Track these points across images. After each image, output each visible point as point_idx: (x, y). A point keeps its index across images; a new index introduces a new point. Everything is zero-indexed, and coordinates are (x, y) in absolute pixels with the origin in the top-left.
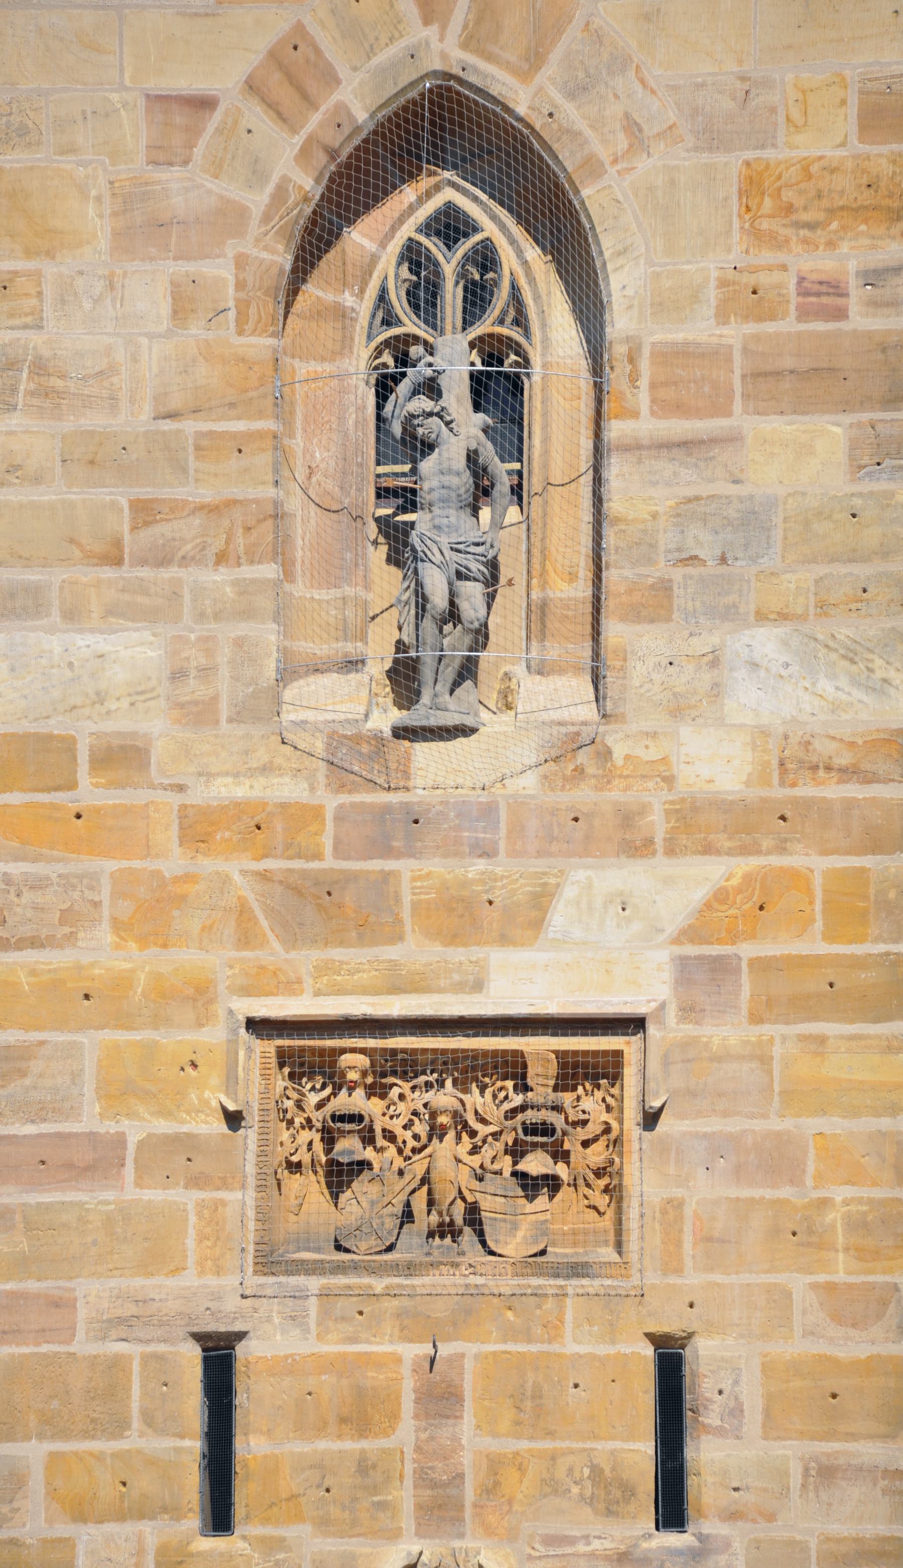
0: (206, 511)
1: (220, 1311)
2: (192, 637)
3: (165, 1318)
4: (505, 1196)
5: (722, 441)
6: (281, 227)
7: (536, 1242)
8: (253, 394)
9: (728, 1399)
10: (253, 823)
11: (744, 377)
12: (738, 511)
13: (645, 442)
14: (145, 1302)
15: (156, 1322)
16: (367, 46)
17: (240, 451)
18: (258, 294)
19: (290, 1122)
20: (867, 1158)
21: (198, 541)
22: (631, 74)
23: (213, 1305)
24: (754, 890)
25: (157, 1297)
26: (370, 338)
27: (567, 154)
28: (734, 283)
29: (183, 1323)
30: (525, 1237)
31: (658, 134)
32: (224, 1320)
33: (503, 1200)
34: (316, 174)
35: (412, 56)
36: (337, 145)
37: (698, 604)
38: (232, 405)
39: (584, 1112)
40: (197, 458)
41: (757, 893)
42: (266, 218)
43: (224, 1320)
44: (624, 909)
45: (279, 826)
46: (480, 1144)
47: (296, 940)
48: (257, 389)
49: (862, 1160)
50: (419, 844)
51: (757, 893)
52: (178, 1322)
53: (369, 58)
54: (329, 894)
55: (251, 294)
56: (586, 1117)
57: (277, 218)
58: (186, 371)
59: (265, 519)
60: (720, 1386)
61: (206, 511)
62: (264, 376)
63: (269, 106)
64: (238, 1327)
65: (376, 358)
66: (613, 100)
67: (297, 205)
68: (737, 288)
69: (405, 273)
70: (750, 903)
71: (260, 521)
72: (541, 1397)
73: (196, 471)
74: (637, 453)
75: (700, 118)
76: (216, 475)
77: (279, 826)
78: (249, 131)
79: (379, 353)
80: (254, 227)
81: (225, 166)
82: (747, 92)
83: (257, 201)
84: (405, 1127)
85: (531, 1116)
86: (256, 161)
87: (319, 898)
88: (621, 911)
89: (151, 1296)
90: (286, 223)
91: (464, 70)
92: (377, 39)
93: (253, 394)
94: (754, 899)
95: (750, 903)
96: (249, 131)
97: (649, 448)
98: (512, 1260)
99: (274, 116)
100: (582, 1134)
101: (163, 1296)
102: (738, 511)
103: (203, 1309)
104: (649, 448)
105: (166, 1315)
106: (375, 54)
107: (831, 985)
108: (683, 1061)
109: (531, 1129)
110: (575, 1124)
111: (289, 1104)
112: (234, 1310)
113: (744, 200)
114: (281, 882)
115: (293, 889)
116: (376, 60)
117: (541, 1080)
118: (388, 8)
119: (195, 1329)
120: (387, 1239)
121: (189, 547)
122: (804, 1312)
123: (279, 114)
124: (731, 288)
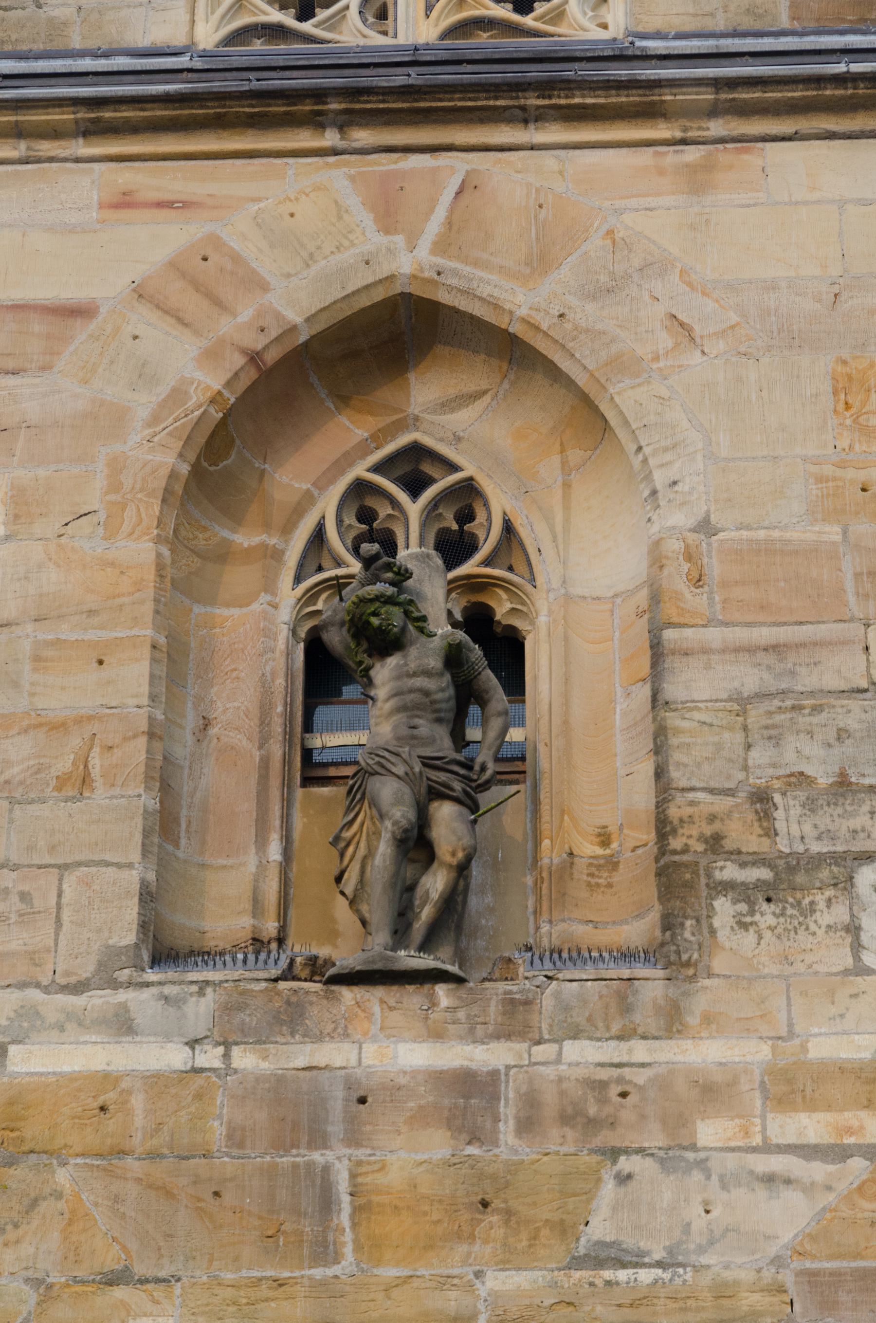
0: (45, 729)
2: (33, 366)
5: (830, 643)
6: (176, 428)
8: (126, 600)
10: (96, 1104)
11: (857, 576)
12: (860, 721)
13: (714, 646)
16: (304, 254)
17: (101, 662)
18: (139, 496)
21: (32, 763)
22: (675, 277)
26: (298, 579)
27: (587, 352)
28: (835, 479)
31: (715, 334)
34: (229, 375)
35: (367, 263)
36: (259, 347)
37: (807, 828)
38: (91, 613)
40: (35, 670)
42: (155, 419)
44: (707, 1212)
45: (138, 1102)
47: (161, 1256)
48: (131, 594)
50: (368, 1128)
53: (308, 266)
55: (129, 496)
57: (171, 420)
58: (26, 578)
59: (135, 736)
61: (45, 729)
62: (142, 580)
63: (166, 312)
65: (307, 604)
66: (650, 301)
67: (201, 406)
68: (841, 484)
69: (350, 519)
71: (126, 739)
73: (32, 684)
74: (705, 657)
75: (773, 319)
76: (63, 688)
77: (138, 1102)
78: (136, 337)
79: (311, 596)
80: (137, 435)
81: (100, 370)
82: (836, 295)
83: (144, 403)
86: (143, 365)
87: (199, 1200)
88: (703, 1214)
90: (183, 425)
91: (439, 274)
92: (319, 248)
93: (126, 600)
96: (136, 337)
97: (723, 651)
99: (173, 321)
102: (860, 721)
104: (723, 651)
106: (316, 262)
113: (842, 396)
114: (139, 1180)
115: (158, 1188)
116: (315, 269)
118: (334, 220)
121: (16, 770)
123: (181, 321)
124: (830, 484)
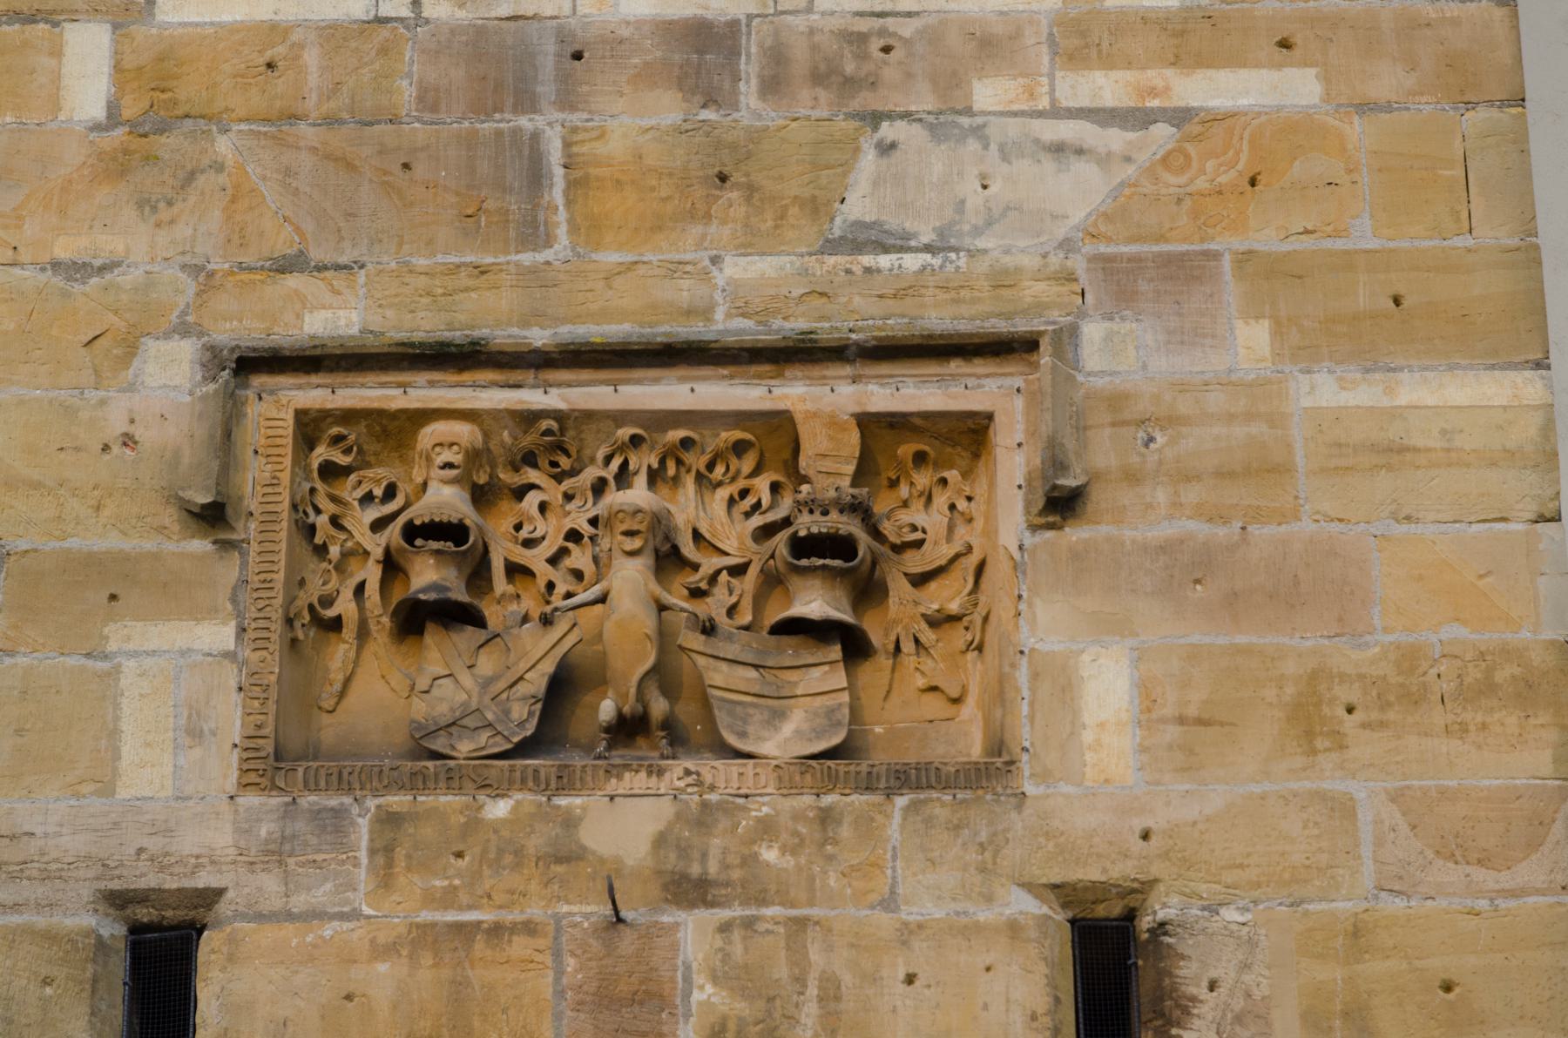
1: (167, 854)
3: (54, 866)
4: (756, 667)
7: (819, 734)
9: (1231, 994)
10: (262, 60)
14: (12, 837)
15: (35, 873)
19: (321, 551)
20: (1489, 580)
23: (154, 845)
24: (1238, 153)
25: (38, 831)
29: (91, 874)
30: (797, 732)
32: (176, 870)
33: (753, 674)
39: (914, 528)
41: (1244, 157)
43: (176, 870)
44: (985, 187)
46: (703, 585)
49: (1481, 583)
50: (585, 88)
51: (1244, 157)
52: (82, 873)
54: (406, 166)
56: (918, 535)
60: (1213, 974)
64: (204, 880)
70: (1233, 174)
72: (838, 998)
84: (553, 561)
85: (807, 524)
87: (386, 173)
88: (980, 189)
89: (27, 828)
94: (1240, 167)
95: (1233, 174)
98: (774, 762)
100: (915, 562)
101: (51, 829)
103: (132, 851)
105: (56, 860)
107: (1397, 301)
108: (1113, 424)
109: (803, 547)
110: (899, 549)
111: (322, 521)
112: (196, 851)
114: (314, 150)
115: (336, 160)
117: (828, 465)
119: (115, 885)
120: (514, 734)
122: (1379, 843)
